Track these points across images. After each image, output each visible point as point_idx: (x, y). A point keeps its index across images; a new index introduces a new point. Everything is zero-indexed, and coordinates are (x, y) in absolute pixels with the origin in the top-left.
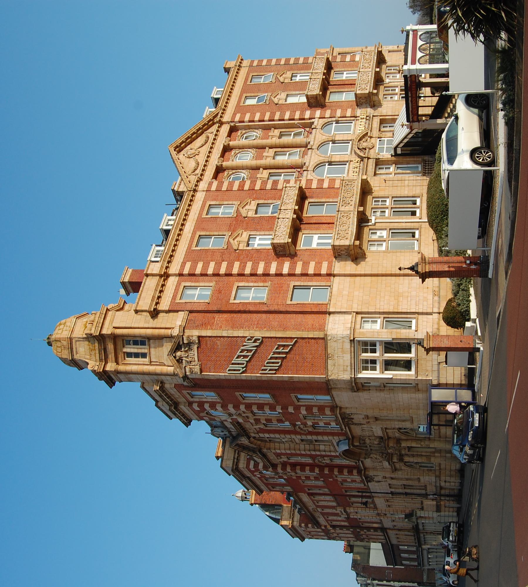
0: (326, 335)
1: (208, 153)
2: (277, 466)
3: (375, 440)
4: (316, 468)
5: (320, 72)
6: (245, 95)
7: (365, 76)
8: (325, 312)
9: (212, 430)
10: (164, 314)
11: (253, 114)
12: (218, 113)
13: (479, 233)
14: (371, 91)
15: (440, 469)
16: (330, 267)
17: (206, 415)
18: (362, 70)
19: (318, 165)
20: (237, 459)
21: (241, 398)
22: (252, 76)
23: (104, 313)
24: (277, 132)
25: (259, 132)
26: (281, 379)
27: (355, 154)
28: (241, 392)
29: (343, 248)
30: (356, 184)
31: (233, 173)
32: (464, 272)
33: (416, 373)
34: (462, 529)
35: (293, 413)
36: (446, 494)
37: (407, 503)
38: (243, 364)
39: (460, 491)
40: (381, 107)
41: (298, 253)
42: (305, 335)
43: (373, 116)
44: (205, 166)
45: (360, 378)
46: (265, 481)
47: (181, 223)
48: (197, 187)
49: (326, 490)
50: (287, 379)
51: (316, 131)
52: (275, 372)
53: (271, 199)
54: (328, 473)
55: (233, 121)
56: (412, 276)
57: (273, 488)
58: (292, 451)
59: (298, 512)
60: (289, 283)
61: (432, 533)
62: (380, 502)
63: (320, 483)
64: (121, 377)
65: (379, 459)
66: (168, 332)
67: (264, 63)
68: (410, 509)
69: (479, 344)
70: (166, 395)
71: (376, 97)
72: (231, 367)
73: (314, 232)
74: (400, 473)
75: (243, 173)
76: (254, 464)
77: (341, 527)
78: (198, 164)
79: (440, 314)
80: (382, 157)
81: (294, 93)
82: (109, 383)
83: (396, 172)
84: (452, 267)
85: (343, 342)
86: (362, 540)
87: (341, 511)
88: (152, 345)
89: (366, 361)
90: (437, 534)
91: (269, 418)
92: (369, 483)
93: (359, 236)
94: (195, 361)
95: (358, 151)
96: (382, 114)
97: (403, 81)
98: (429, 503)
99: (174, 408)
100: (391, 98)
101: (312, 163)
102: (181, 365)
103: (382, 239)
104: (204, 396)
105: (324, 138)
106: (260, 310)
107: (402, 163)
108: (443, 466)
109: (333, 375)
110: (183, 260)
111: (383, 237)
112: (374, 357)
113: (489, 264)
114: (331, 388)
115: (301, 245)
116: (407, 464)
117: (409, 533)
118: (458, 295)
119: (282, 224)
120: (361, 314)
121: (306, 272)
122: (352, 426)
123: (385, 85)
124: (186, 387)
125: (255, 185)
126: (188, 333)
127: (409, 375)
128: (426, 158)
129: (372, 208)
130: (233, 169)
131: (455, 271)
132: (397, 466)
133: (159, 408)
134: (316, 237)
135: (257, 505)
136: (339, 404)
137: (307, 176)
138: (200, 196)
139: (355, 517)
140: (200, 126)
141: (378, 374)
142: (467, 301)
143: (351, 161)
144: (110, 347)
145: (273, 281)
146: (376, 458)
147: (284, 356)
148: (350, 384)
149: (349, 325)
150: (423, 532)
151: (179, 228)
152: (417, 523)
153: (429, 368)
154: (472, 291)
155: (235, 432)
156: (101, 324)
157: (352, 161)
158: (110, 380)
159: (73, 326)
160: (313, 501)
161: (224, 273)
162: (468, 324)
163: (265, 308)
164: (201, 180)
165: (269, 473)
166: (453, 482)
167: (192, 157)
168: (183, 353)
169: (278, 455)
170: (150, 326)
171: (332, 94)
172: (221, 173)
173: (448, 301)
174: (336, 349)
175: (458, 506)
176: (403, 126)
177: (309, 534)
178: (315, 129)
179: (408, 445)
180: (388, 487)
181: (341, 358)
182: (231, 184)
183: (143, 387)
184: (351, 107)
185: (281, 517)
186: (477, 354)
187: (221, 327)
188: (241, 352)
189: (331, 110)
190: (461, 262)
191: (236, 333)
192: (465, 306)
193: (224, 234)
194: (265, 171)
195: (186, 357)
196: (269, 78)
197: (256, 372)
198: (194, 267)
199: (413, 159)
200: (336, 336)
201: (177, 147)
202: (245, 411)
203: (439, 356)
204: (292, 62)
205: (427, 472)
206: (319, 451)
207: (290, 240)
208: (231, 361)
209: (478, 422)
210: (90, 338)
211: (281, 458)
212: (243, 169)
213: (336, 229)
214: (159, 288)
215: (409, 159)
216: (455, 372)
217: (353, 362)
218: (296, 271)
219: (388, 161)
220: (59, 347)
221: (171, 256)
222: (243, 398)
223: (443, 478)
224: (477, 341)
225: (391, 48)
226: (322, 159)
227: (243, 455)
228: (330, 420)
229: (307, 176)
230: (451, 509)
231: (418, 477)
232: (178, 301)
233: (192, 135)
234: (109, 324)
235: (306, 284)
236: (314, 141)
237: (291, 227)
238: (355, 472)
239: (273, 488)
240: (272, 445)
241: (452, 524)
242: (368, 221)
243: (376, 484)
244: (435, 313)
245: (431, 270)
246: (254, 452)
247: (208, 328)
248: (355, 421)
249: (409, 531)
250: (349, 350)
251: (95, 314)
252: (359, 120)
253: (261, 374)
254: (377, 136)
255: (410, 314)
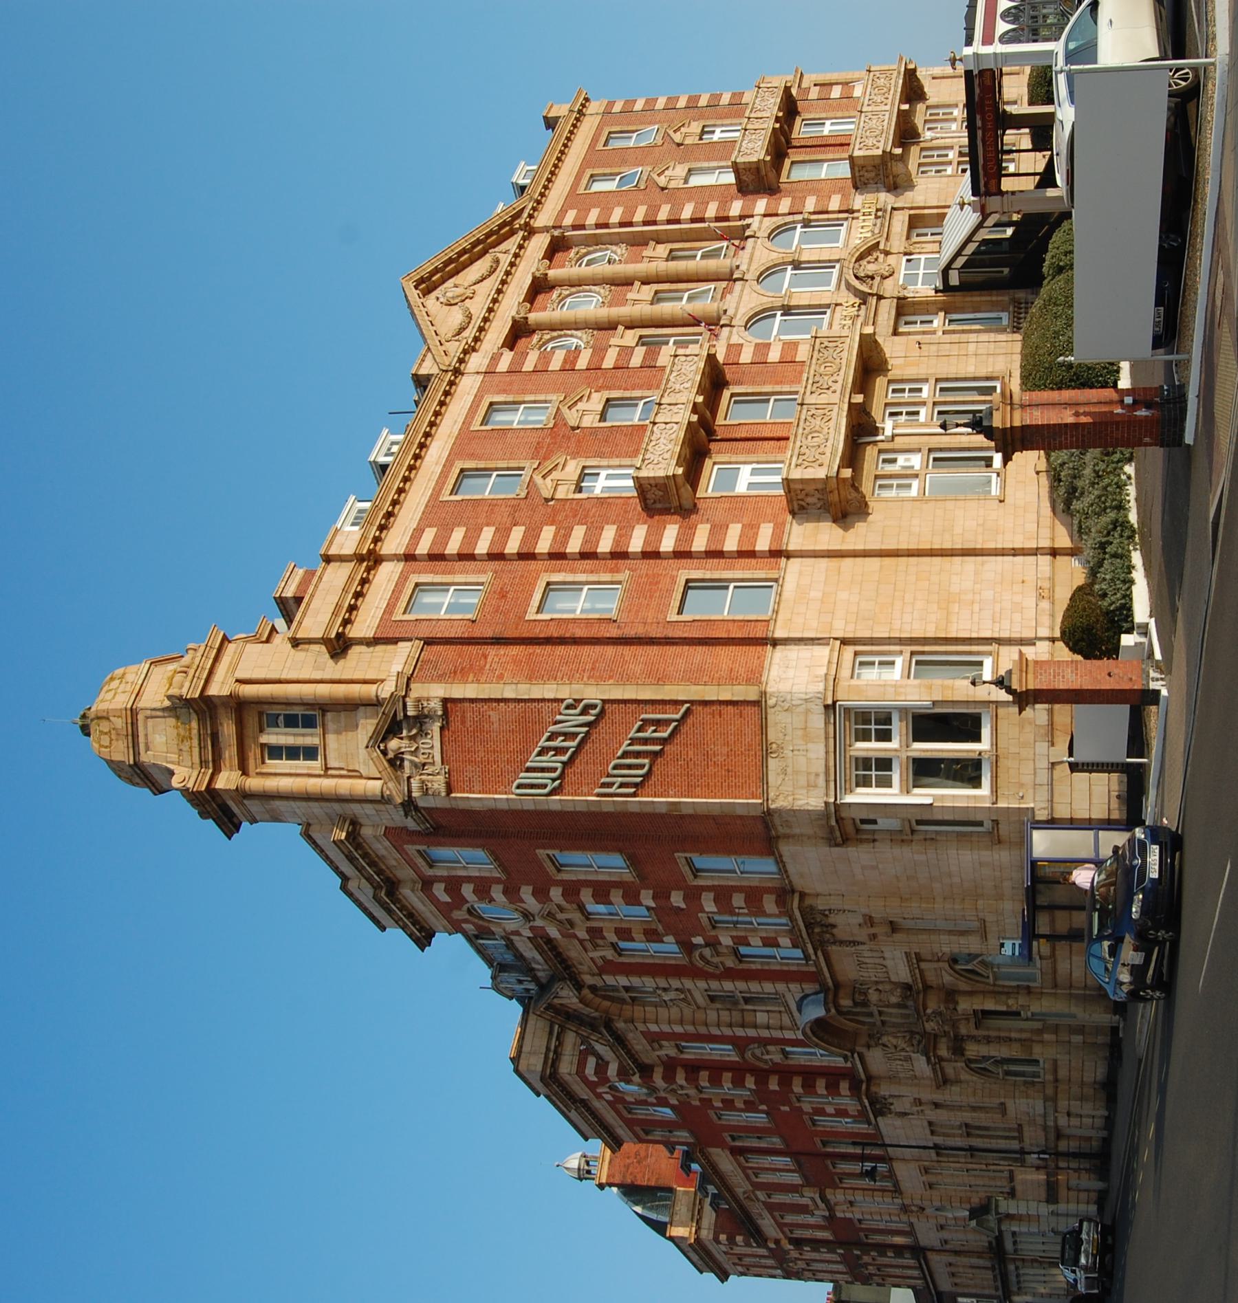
0: (764, 694)
1: (493, 292)
2: (653, 1071)
3: (891, 992)
4: (748, 1075)
5: (768, 115)
6: (589, 172)
7: (874, 121)
8: (762, 639)
9: (494, 978)
10: (363, 648)
11: (608, 211)
12: (522, 210)
13: (1156, 324)
14: (888, 150)
15: (1056, 1080)
16: (778, 534)
17: (467, 917)
18: (870, 109)
19: (756, 314)
20: (555, 1052)
21: (553, 868)
22: (610, 133)
23: (217, 646)
24: (662, 250)
25: (619, 251)
26: (648, 809)
27: (848, 289)
28: (553, 848)
29: (810, 488)
30: (846, 346)
31: (552, 339)
32: (1117, 429)
33: (992, 792)
34: (1110, 1240)
35: (683, 909)
36: (1071, 1150)
37: (975, 1176)
38: (555, 770)
39: (1107, 1142)
40: (912, 190)
41: (699, 506)
42: (711, 693)
43: (893, 209)
44: (486, 320)
45: (850, 804)
46: (625, 1113)
47: (417, 441)
48: (463, 365)
49: (776, 1142)
50: (664, 810)
51: (756, 242)
52: (633, 790)
53: (641, 387)
54: (777, 1088)
55: (559, 224)
56: (982, 555)
57: (647, 1133)
58: (686, 1027)
59: (711, 1205)
60: (674, 573)
61: (1036, 1261)
62: (907, 1174)
63: (759, 1118)
64: (254, 806)
65: (903, 1050)
66: (370, 690)
67: (639, 106)
68: (983, 1195)
69: (1157, 680)
70: (365, 856)
71: (900, 165)
72: (525, 778)
73: (741, 458)
74: (955, 1089)
75: (576, 337)
76: (597, 1064)
77: (816, 1244)
78: (470, 317)
79: (1053, 642)
80: (912, 295)
81: (705, 164)
82: (224, 823)
83: (947, 327)
84: (1086, 414)
85: (808, 711)
86: (866, 1280)
87: (812, 1199)
88: (331, 726)
89: (865, 763)
90: (1050, 1263)
91: (624, 925)
92: (879, 1119)
93: (853, 456)
94: (433, 764)
95: (856, 283)
96: (914, 205)
97: (966, 134)
98: (1030, 1178)
99: (387, 895)
100: (938, 171)
101: (742, 311)
102: (399, 773)
103: (909, 472)
104: (461, 863)
105: (774, 257)
106: (600, 635)
107: (961, 310)
108: (1063, 1073)
109: (781, 797)
110: (419, 524)
111: (912, 467)
112: (885, 750)
113: (1186, 405)
114: (778, 837)
115: (709, 486)
116: (973, 1066)
117: (981, 1262)
118: (1102, 570)
119: (663, 436)
120: (855, 644)
121: (719, 548)
122: (833, 949)
123: (922, 145)
124: (413, 836)
125: (603, 359)
126: (417, 690)
127: (978, 796)
128: (1021, 295)
129: (886, 405)
130: (552, 327)
131: (1094, 423)
132: (949, 1069)
133: (350, 895)
134: (746, 470)
135: (615, 1189)
136: (798, 883)
137: (729, 338)
138: (468, 386)
139: (849, 1215)
140: (480, 236)
141: (895, 795)
142: (1124, 582)
143: (837, 305)
144: (228, 730)
145: (636, 570)
146: (896, 1047)
147: (658, 748)
148: (824, 822)
149: (823, 671)
150: (1014, 1260)
151: (412, 453)
152: (1000, 1232)
153: (1027, 779)
154: (1137, 558)
155: (544, 970)
156: (207, 671)
157: (841, 305)
158: (226, 816)
159: (140, 682)
160: (744, 1169)
161: (515, 551)
162: (1127, 640)
163: (614, 632)
164: (474, 350)
165: (632, 1089)
166: (1088, 1116)
167: (456, 304)
168: (406, 742)
169: (655, 1039)
170: (327, 676)
171: (795, 167)
172: (524, 339)
173: (1075, 591)
174: (789, 731)
175: (1100, 1185)
176: (962, 205)
177: (737, 1261)
178: (753, 239)
179: (976, 1007)
180: (928, 1131)
181: (801, 752)
182: (545, 358)
183: (307, 836)
184: (841, 190)
185: (672, 1217)
186: (1153, 708)
187: (501, 677)
188: (549, 739)
189: (794, 198)
190: (1111, 403)
191: (537, 691)
192: (1119, 595)
193: (521, 465)
194: (630, 333)
195: (412, 753)
196: (650, 134)
197: (585, 789)
198: (442, 538)
199: (988, 298)
200: (789, 697)
201: (421, 281)
202: (564, 903)
203: (1053, 745)
204: (703, 102)
205: (1022, 1088)
206: (755, 1026)
207: (680, 471)
208: (525, 763)
209: (1157, 867)
210: (180, 707)
211: (661, 1047)
212: (577, 329)
213: (794, 442)
214: (355, 587)
215: (978, 299)
216: (1093, 787)
217: (832, 763)
218: (694, 544)
219: (927, 303)
220: (106, 733)
221: (389, 515)
222: (556, 867)
223: (1063, 1104)
224: (1152, 674)
225: (937, 71)
226: (766, 302)
227: (570, 1039)
228: (776, 931)
229: (729, 338)
230: (1083, 1196)
231: (1002, 1100)
232: (398, 615)
233: (460, 254)
234: (227, 672)
235: (716, 575)
236: (749, 265)
237: (683, 442)
238: (844, 1086)
239: (647, 1133)
240: (638, 1011)
241: (1085, 1224)
242: (875, 431)
243: (898, 1122)
244: (1041, 639)
245: (1028, 423)
246: (594, 1028)
247: (470, 679)
248: (839, 933)
249: (979, 1255)
250: (822, 732)
251: (195, 650)
252: (857, 218)
253: (598, 795)
254: (902, 250)
255: (978, 645)
